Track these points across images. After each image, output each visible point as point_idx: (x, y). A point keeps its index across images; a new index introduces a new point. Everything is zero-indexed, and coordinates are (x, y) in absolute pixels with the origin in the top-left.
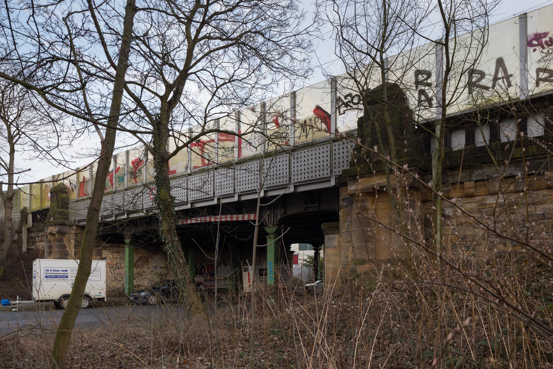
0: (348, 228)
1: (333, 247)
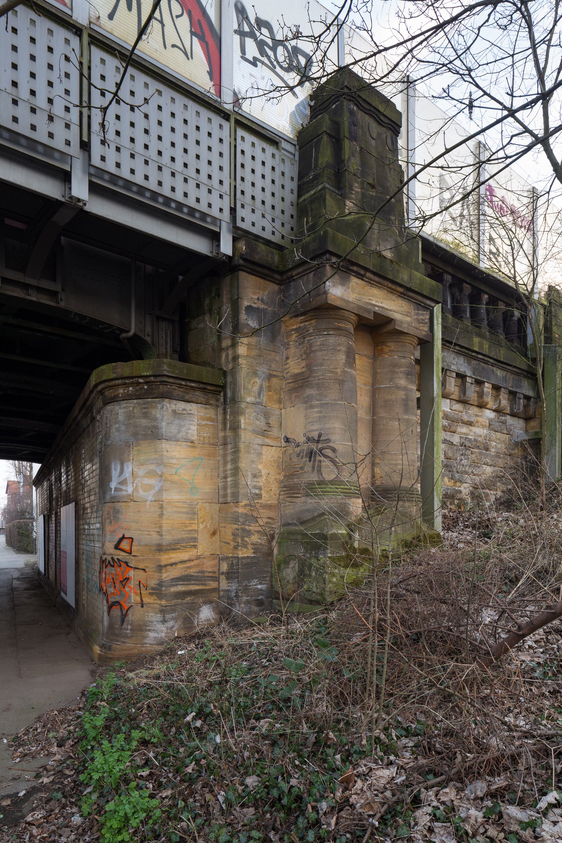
0: (259, 394)
1: (187, 440)
